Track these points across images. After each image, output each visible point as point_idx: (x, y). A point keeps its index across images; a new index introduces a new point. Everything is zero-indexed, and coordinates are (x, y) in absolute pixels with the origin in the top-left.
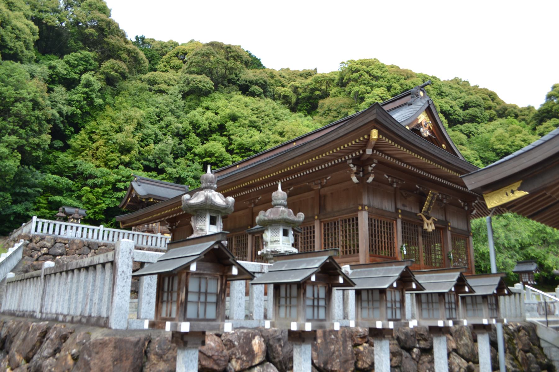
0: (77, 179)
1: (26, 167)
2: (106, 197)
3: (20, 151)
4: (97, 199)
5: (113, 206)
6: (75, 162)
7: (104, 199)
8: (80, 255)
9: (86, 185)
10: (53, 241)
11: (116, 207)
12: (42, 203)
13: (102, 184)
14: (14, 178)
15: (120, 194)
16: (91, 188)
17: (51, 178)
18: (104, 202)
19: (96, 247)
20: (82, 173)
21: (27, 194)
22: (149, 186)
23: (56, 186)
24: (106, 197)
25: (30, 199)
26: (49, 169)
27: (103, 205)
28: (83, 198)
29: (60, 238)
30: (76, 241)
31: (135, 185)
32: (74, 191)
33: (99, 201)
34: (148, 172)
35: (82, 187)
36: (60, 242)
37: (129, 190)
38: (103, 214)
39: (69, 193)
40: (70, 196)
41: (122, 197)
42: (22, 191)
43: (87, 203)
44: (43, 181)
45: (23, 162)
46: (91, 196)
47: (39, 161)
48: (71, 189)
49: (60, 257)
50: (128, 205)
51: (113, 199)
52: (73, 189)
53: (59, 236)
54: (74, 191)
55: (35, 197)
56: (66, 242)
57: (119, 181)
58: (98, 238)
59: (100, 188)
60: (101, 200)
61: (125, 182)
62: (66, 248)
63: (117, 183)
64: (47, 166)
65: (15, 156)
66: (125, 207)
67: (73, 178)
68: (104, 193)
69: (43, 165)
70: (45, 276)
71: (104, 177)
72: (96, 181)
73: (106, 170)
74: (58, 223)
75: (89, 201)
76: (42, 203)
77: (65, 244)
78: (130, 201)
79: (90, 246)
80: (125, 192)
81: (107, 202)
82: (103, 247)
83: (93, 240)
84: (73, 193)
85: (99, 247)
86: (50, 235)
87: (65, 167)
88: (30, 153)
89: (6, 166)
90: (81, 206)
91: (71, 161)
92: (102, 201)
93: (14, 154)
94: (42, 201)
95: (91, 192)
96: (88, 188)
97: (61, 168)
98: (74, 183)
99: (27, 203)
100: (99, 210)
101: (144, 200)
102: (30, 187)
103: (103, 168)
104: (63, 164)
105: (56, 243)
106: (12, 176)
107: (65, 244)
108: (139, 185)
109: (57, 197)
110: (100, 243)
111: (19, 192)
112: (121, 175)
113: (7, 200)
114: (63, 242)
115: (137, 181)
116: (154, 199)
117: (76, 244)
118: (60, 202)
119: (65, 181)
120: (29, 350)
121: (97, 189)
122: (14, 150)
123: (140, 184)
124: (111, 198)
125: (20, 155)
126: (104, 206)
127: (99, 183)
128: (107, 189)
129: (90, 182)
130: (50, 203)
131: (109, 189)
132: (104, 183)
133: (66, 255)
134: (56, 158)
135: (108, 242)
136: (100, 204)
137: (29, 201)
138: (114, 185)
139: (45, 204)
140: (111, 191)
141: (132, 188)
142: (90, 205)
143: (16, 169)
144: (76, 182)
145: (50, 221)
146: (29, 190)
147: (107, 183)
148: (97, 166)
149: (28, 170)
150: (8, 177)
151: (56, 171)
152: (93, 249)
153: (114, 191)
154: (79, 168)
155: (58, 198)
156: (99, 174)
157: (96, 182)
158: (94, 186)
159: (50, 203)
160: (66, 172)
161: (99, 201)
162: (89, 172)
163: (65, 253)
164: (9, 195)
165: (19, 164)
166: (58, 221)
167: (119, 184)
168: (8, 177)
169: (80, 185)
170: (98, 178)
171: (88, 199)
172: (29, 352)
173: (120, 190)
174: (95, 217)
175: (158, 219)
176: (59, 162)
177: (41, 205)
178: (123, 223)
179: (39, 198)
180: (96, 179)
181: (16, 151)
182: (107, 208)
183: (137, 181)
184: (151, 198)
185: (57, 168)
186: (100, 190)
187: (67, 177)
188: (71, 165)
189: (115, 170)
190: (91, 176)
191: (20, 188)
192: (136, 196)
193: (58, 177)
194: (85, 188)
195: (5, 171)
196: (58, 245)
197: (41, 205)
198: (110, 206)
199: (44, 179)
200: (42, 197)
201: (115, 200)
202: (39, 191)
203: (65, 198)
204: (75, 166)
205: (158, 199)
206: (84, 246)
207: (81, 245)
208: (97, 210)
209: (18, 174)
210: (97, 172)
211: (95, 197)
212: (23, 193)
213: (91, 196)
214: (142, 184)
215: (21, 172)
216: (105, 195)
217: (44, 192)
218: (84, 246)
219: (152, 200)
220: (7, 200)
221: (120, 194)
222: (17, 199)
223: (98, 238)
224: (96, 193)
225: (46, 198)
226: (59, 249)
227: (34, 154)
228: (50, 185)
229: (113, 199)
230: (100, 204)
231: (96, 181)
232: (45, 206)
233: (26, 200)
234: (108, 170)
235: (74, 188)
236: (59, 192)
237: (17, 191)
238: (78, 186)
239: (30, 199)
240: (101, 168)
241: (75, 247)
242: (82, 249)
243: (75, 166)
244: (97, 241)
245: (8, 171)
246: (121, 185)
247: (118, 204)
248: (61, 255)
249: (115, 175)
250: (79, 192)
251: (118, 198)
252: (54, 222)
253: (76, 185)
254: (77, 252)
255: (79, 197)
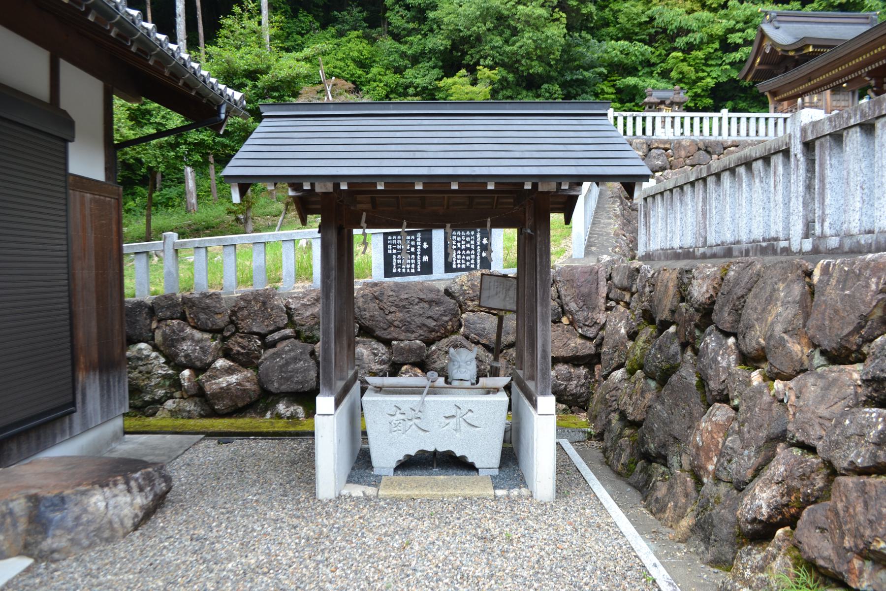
0: (656, 42)
1: (577, 35)
2: (711, 65)
3: (563, 9)
4: (697, 72)
5: (725, 80)
6: (649, 12)
7: (708, 69)
8: (693, 166)
9: (675, 49)
10: (645, 146)
11: (732, 80)
12: (607, 93)
13: (701, 42)
14: (561, 56)
15: (737, 56)
16: (683, 51)
17: (614, 49)
18: (709, 75)
19: (719, 149)
20: (665, 30)
21: (583, 82)
22: (795, 25)
23: (626, 61)
24: (711, 65)
25: (589, 90)
26: (608, 34)
27: (709, 80)
28: (674, 74)
29: (656, 141)
30: (684, 143)
31: (768, 29)
32: (654, 65)
33: (701, 74)
34: (783, 4)
35: (667, 55)
36: (657, 148)
37: (756, 44)
38: (709, 97)
39: (647, 69)
40: (651, 74)
41: (741, 61)
42: (575, 77)
43: (680, 81)
44: (605, 55)
45: (569, 27)
46: (685, 67)
47: (592, 22)
48: (649, 61)
49: (660, 173)
50: (758, 71)
51: (724, 67)
52: (652, 61)
53: (654, 137)
54: (654, 65)
55: (594, 85)
56: (667, 146)
57: (732, 31)
58: (720, 134)
59: (700, 49)
60: (703, 71)
61: (743, 30)
62: (668, 156)
63: (729, 36)
64: (604, 31)
65: (557, 20)
66: (750, 77)
67: (650, 41)
68: (708, 58)
69: (598, 29)
70: (808, 146)
71: (704, 29)
72: (690, 38)
73: (706, 15)
74: (649, 115)
75: (684, 77)
76: (607, 93)
77: (666, 150)
78: (760, 64)
79: (709, 149)
80: (747, 50)
81: (714, 75)
82: (732, 148)
83: (712, 138)
84: (653, 69)
85: (725, 149)
86: (638, 138)
87: (633, 25)
88: (578, 10)
89: (547, 37)
90: (670, 87)
91: (643, 13)
92: (705, 74)
93: (556, 16)
94: (606, 89)
95: (684, 60)
96: (680, 54)
97: (627, 29)
98: (653, 50)
99: (584, 96)
100: (703, 90)
101: (792, 54)
102: (586, 70)
103: (701, 13)
104: (628, 20)
105: (650, 150)
106: (558, 54)
107: (666, 150)
108: (778, 28)
109: (630, 78)
110: (726, 142)
111: (572, 80)
112: (733, 18)
113: (556, 96)
114: (662, 146)
115: (771, 21)
116: (814, 46)
117: (685, 148)
118: (635, 87)
119: (638, 48)
120: (851, 328)
121: (694, 53)
122: (554, 8)
123: (777, 25)
124: (721, 65)
125: (564, 15)
126: (710, 82)
127: (698, 41)
128: (712, 51)
129: (681, 42)
130: (619, 91)
131: (716, 50)
132: (705, 40)
133: (671, 169)
134: (615, 12)
135: (739, 138)
136: (703, 78)
137: (587, 93)
138: (723, 40)
139: (612, 93)
140: (719, 53)
141: (763, 36)
142: (686, 83)
143: (562, 41)
144: (656, 48)
145: (635, 114)
146: (587, 74)
147: (711, 38)
148: (690, 12)
149: (580, 41)
150: (552, 56)
151: (620, 35)
152: (714, 153)
153: (724, 52)
154: (658, 21)
155: (631, 81)
156: (695, 25)
157: (692, 40)
158: (690, 48)
159: (619, 91)
160: (636, 34)
161: (701, 74)
162: (676, 24)
163: (668, 166)
164: (557, 87)
165: (565, 31)
166: (648, 111)
167: (733, 36)
168: (552, 56)
169: (664, 52)
170: (694, 32)
171: (681, 73)
172: (851, 334)
173: (736, 47)
174: (696, 104)
175: (826, 84)
176: (622, 19)
177: (606, 96)
178: (774, 94)
179: (601, 86)
180: (690, 35)
181: (557, 9)
182: (716, 84)
183: (771, 21)
184: (808, 46)
185: (621, 30)
186: (700, 54)
187: (640, 41)
188: (644, 19)
189: (722, 12)
190: (683, 31)
191: (572, 73)
192: (772, 50)
193: (626, 43)
194: (674, 54)
195: (546, 47)
196: (654, 152)
197: (606, 96)
198: (720, 80)
199: (606, 52)
200: (606, 82)
201: (728, 67)
202: (600, 74)
203: (642, 78)
204: (652, 19)
205: (824, 46)
206: (699, 149)
207: (693, 149)
208: (699, 91)
209: (566, 49)
210: (690, 21)
211: (692, 68)
212: (577, 80)
213: (685, 67)
214: (782, 25)
215: (569, 45)
216: (710, 62)
217: (609, 72)
218: (699, 149)
219: (811, 49)
220: (556, 96)
221: (737, 56)
222: (569, 92)
223: (720, 134)
224: (694, 60)
225: (612, 83)
226: (658, 159)
227: (584, 11)
228: (616, 59)
229: (724, 67)
230: (703, 78)
231: (690, 38)
232: (613, 96)
233: (584, 92)
234: (711, 15)
235: (654, 60)
236: (631, 71)
237: (569, 79)
238: (660, 55)
239: (589, 90)
240: (696, 14)
241: (683, 153)
242: (696, 155)
243: (652, 19)
244: (720, 138)
245: (551, 46)
246: (736, 38)
247: (735, 74)
248: (662, 169)
249: (724, 21)
250: (662, 64)
251: (732, 64)
252: (642, 114)
253: (657, 53)
254: (688, 161)
255: (665, 74)
